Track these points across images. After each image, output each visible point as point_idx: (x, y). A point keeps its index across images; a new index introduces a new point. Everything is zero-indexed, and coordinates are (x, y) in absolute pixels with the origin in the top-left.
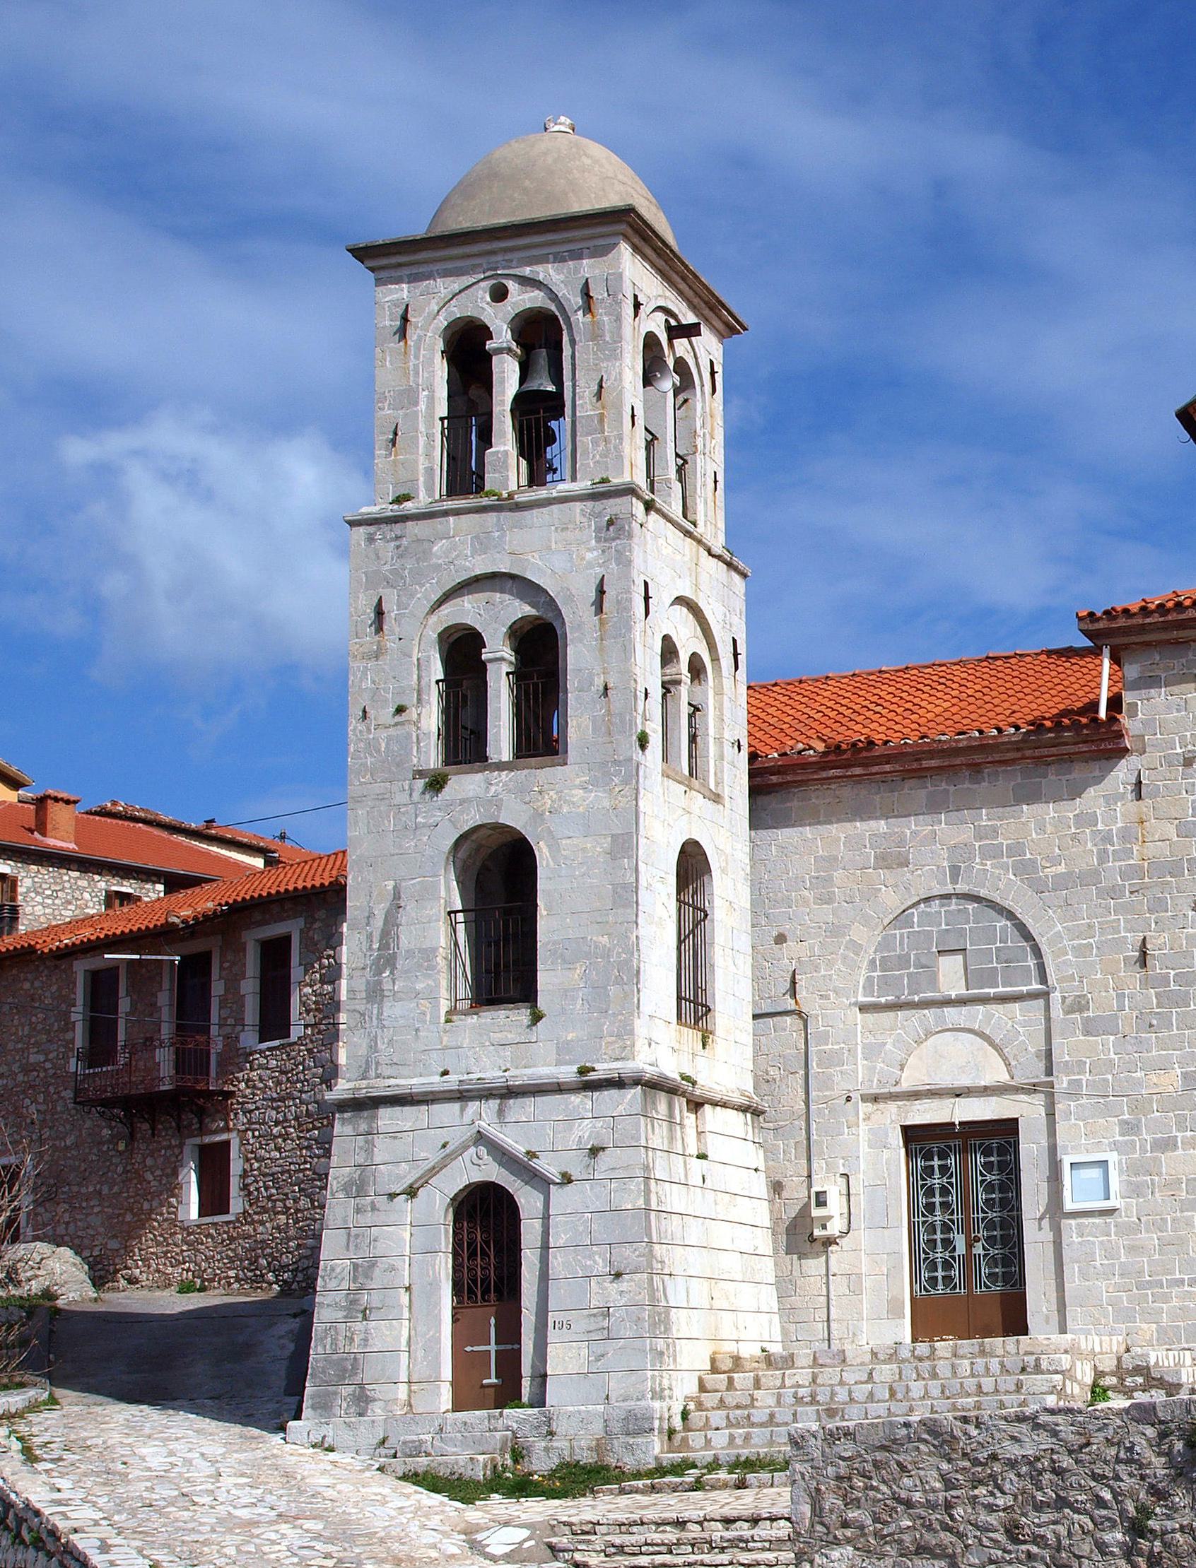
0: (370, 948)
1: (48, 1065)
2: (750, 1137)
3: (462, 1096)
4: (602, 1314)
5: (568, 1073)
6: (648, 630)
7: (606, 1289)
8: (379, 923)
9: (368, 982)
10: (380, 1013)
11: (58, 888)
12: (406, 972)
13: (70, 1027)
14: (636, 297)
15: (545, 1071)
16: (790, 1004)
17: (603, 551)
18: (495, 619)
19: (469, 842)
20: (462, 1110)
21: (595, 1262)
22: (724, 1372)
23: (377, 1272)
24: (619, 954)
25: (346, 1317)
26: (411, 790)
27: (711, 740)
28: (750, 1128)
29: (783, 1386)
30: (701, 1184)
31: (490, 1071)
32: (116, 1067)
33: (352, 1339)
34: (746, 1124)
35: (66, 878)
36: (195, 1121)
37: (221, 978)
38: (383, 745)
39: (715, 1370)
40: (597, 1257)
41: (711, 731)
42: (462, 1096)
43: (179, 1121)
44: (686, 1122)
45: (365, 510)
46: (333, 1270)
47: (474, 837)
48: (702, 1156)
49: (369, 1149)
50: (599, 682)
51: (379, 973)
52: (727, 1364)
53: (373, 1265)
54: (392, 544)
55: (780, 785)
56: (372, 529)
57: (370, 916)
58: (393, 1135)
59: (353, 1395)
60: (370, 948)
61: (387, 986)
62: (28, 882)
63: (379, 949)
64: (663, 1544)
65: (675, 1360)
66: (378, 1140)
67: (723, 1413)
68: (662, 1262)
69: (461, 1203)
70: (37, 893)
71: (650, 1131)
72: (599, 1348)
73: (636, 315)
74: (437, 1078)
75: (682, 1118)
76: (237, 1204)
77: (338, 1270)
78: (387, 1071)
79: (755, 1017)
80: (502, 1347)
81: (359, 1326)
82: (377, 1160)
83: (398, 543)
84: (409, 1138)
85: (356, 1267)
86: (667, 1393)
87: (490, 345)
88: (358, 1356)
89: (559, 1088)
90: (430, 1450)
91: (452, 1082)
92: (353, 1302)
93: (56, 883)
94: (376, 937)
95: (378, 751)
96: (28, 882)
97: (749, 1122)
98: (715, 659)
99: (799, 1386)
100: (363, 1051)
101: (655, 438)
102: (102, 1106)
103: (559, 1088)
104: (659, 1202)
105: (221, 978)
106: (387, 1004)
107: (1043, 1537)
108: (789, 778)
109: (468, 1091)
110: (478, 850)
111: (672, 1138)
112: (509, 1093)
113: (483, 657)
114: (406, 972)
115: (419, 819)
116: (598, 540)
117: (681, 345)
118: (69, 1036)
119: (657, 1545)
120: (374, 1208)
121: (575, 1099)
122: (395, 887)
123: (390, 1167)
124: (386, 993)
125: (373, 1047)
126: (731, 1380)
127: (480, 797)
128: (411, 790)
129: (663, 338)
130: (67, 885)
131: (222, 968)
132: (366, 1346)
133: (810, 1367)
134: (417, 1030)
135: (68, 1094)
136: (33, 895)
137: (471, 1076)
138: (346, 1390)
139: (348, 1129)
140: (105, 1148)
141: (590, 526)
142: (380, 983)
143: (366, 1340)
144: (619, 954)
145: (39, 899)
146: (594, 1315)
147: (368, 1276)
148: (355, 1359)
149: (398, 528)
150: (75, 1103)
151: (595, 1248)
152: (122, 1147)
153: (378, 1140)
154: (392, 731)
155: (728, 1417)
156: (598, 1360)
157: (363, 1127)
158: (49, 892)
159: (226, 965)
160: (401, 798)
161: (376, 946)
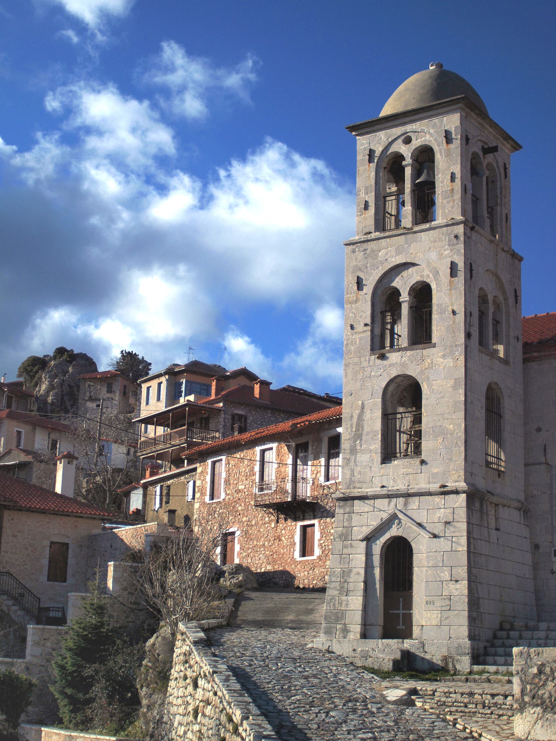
0: (352, 431)
1: (245, 490)
2: (522, 522)
3: (389, 496)
4: (448, 599)
5: (435, 487)
6: (472, 285)
7: (450, 587)
8: (355, 420)
9: (350, 446)
10: (355, 460)
11: (263, 420)
12: (366, 441)
13: (254, 474)
14: (467, 136)
15: (423, 485)
16: (543, 460)
17: (451, 250)
18: (403, 284)
19: (394, 383)
20: (389, 503)
21: (445, 574)
22: (506, 630)
23: (352, 575)
24: (457, 433)
25: (339, 594)
26: (369, 360)
27: (504, 337)
28: (522, 518)
29: (532, 639)
30: (496, 542)
31: (401, 486)
32: (270, 491)
33: (341, 604)
34: (520, 516)
35: (266, 417)
36: (301, 515)
37: (312, 453)
38: (358, 341)
39: (501, 629)
40: (446, 572)
41: (504, 332)
42: (389, 496)
43: (304, 516)
44: (490, 513)
45: (351, 239)
46: (334, 573)
47: (396, 381)
48: (497, 529)
49: (350, 520)
50: (450, 309)
51: (355, 442)
52: (507, 626)
53: (350, 571)
54: (362, 253)
55: (538, 357)
56: (354, 247)
57: (352, 417)
58: (360, 514)
59: (342, 629)
60: (352, 431)
61: (358, 447)
62: (251, 418)
63: (355, 431)
64: (462, 702)
65: (482, 623)
66: (354, 516)
67: (503, 649)
68: (476, 576)
69: (388, 546)
70: (255, 423)
71: (471, 515)
72: (446, 614)
73: (467, 144)
74: (379, 489)
75: (487, 511)
76: (317, 552)
77: (336, 573)
78: (358, 485)
79: (526, 465)
80: (408, 612)
81: (344, 598)
82: (353, 524)
83: (364, 252)
84: (366, 516)
85: (344, 571)
86: (477, 637)
87: (404, 163)
88: (344, 612)
89: (430, 494)
90: (371, 655)
91: (384, 491)
92: (342, 587)
93: (262, 419)
94: (354, 426)
95: (356, 344)
96: (251, 418)
97: (522, 515)
98: (506, 299)
99: (540, 639)
100: (348, 476)
101: (477, 199)
102: (265, 507)
103: (430, 494)
104: (475, 548)
105: (312, 453)
106: (358, 456)
107: (198, 583)
108: (542, 354)
109: (391, 495)
110: (398, 387)
111: (482, 518)
112: (408, 495)
113: (400, 300)
114: (366, 441)
115: (372, 373)
116: (449, 245)
117: (490, 157)
118: (253, 478)
119: (460, 702)
120: (351, 546)
121: (437, 499)
122: (362, 403)
123: (358, 528)
124: (358, 451)
125: (352, 474)
126: (508, 634)
127: (400, 362)
128: (369, 360)
129: (481, 154)
130: (266, 420)
131: (312, 449)
132: (347, 607)
133: (546, 631)
134: (371, 467)
135: (252, 503)
136: (253, 423)
137: (393, 488)
138: (339, 626)
139: (342, 511)
140: (266, 526)
141: (446, 240)
142: (355, 446)
143: (347, 604)
144: (457, 433)
145: (255, 425)
146: (444, 599)
147: (349, 577)
148: (343, 613)
149: (365, 245)
150: (255, 506)
151: (445, 568)
152: (273, 525)
153: (354, 516)
154: (362, 335)
155: (505, 651)
156: (445, 620)
157: (348, 510)
158: (259, 423)
159: (314, 448)
160: (365, 364)
161: (354, 430)
